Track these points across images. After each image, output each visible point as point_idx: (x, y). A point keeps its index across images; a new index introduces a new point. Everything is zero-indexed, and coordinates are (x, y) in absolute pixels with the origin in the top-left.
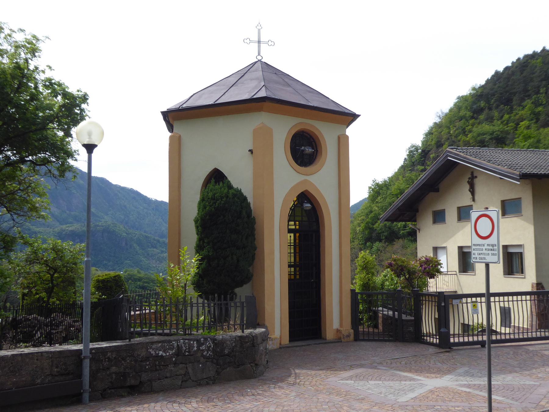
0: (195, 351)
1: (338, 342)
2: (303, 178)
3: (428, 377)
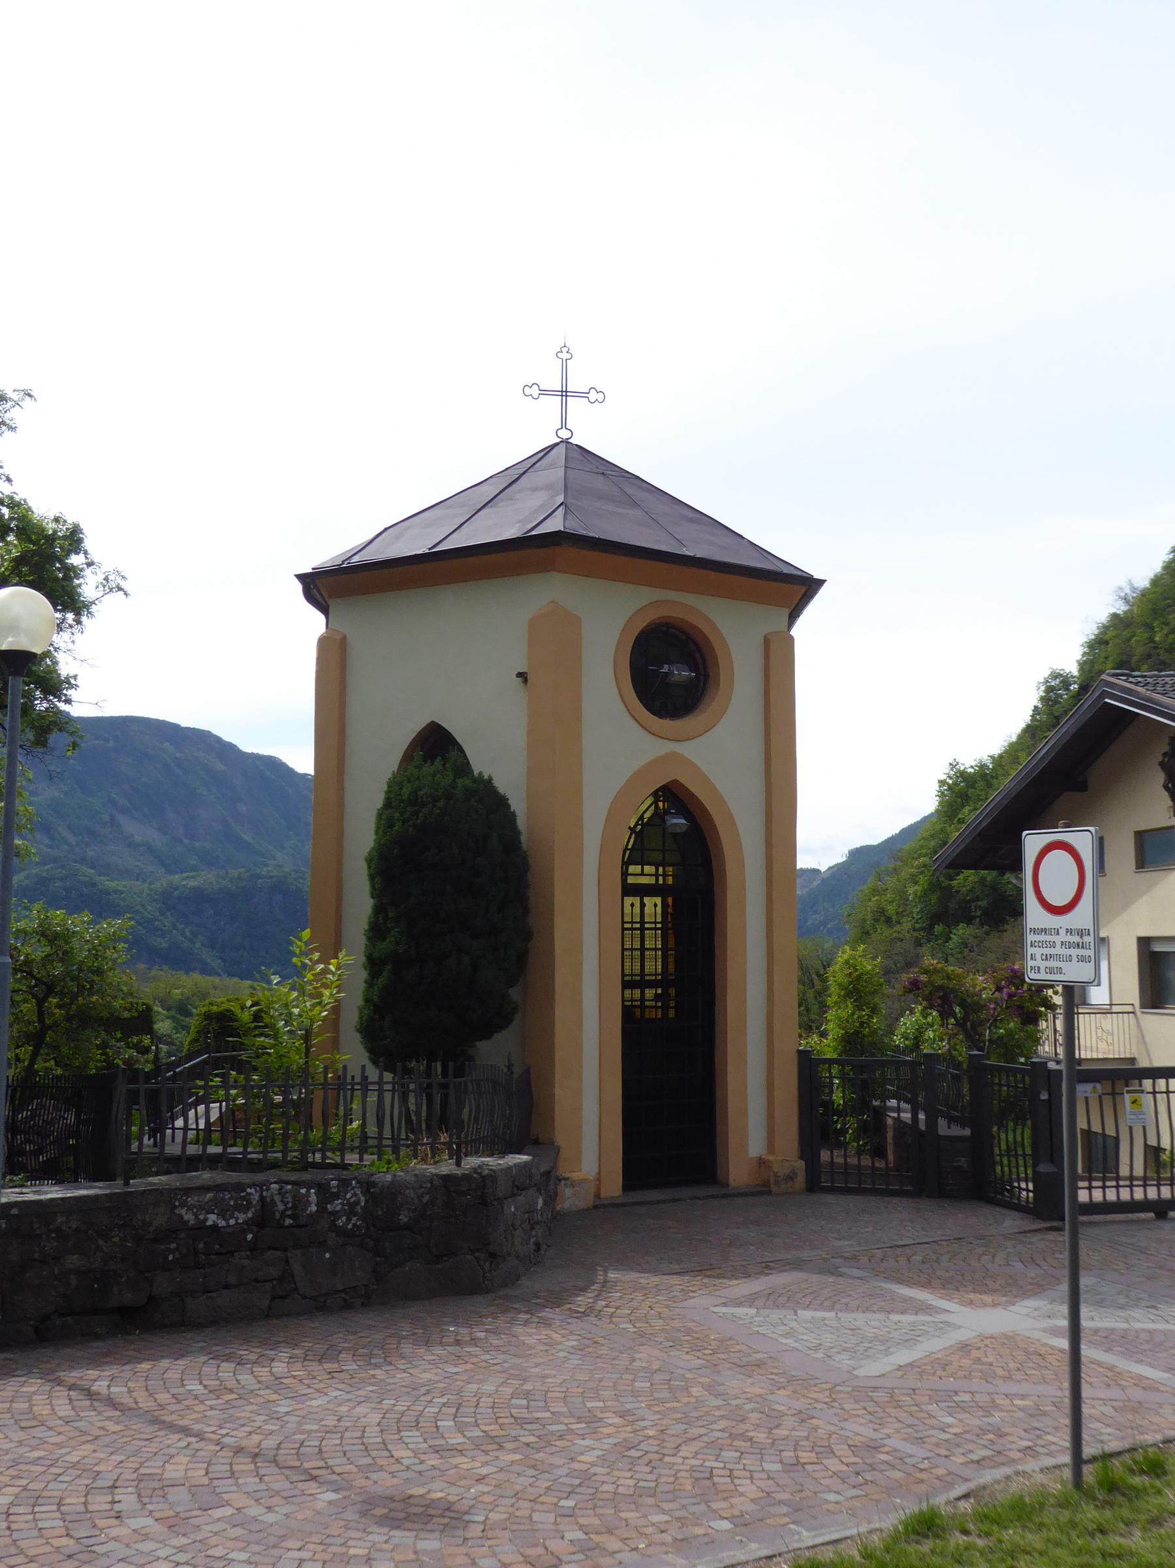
0: (311, 1215)
1: (761, 1193)
3: (971, 1303)
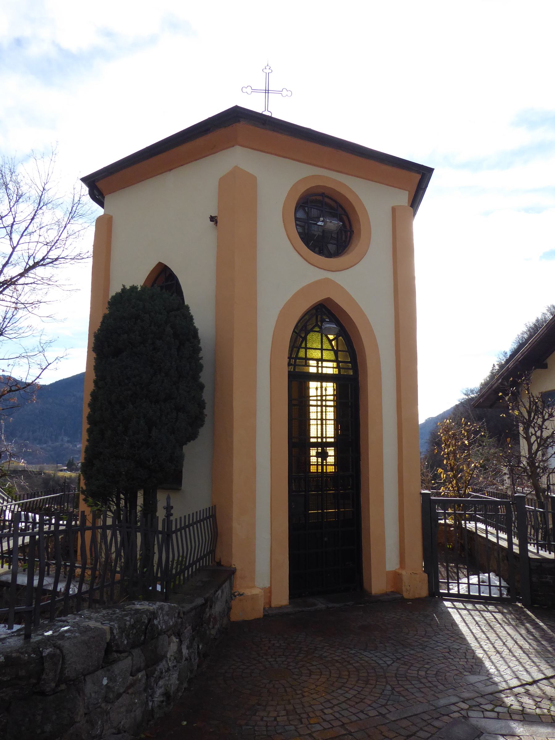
2: (322, 275)
